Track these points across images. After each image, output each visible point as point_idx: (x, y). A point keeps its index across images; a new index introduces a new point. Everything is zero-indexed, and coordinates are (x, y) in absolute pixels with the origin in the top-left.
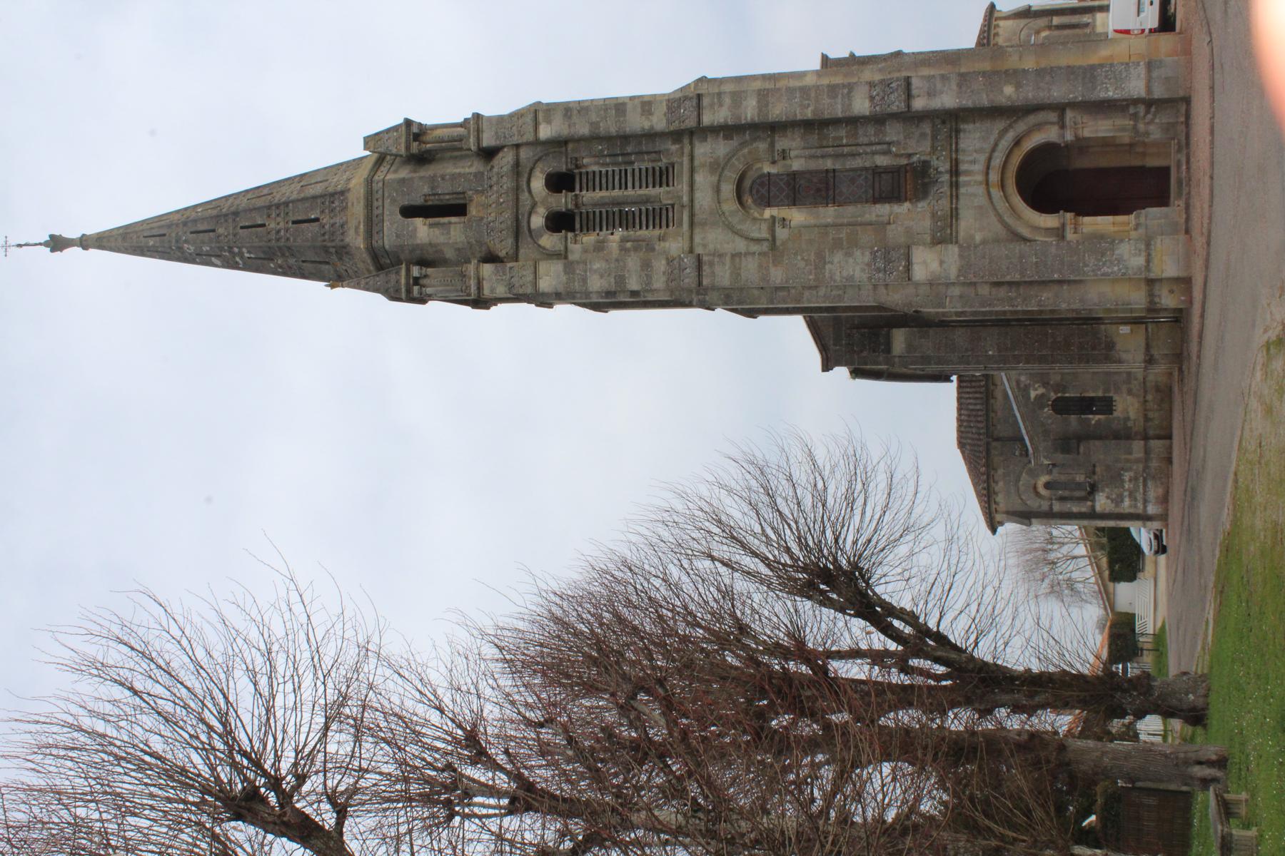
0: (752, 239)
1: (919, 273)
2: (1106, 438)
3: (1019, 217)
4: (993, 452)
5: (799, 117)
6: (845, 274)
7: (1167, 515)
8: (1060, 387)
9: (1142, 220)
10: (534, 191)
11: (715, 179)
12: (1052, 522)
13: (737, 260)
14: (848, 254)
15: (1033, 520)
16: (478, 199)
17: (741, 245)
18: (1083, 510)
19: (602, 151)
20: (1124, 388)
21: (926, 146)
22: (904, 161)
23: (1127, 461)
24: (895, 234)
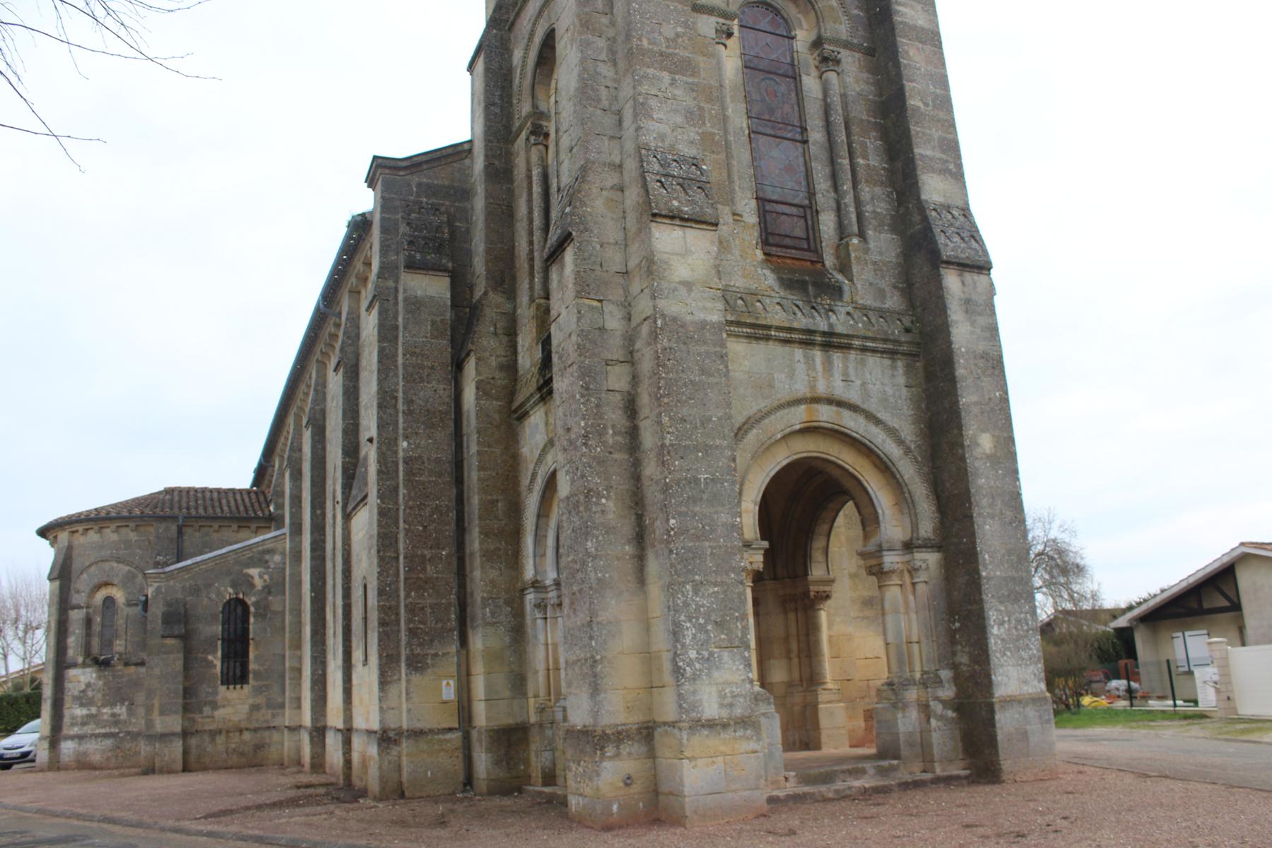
1: (666, 238)
2: (187, 677)
4: (162, 527)
5: (908, 86)
6: (653, 103)
7: (59, 769)
12: (54, 610)
15: (57, 583)
18: (71, 652)
20: (261, 700)
21: (867, 299)
22: (829, 260)
23: (149, 710)
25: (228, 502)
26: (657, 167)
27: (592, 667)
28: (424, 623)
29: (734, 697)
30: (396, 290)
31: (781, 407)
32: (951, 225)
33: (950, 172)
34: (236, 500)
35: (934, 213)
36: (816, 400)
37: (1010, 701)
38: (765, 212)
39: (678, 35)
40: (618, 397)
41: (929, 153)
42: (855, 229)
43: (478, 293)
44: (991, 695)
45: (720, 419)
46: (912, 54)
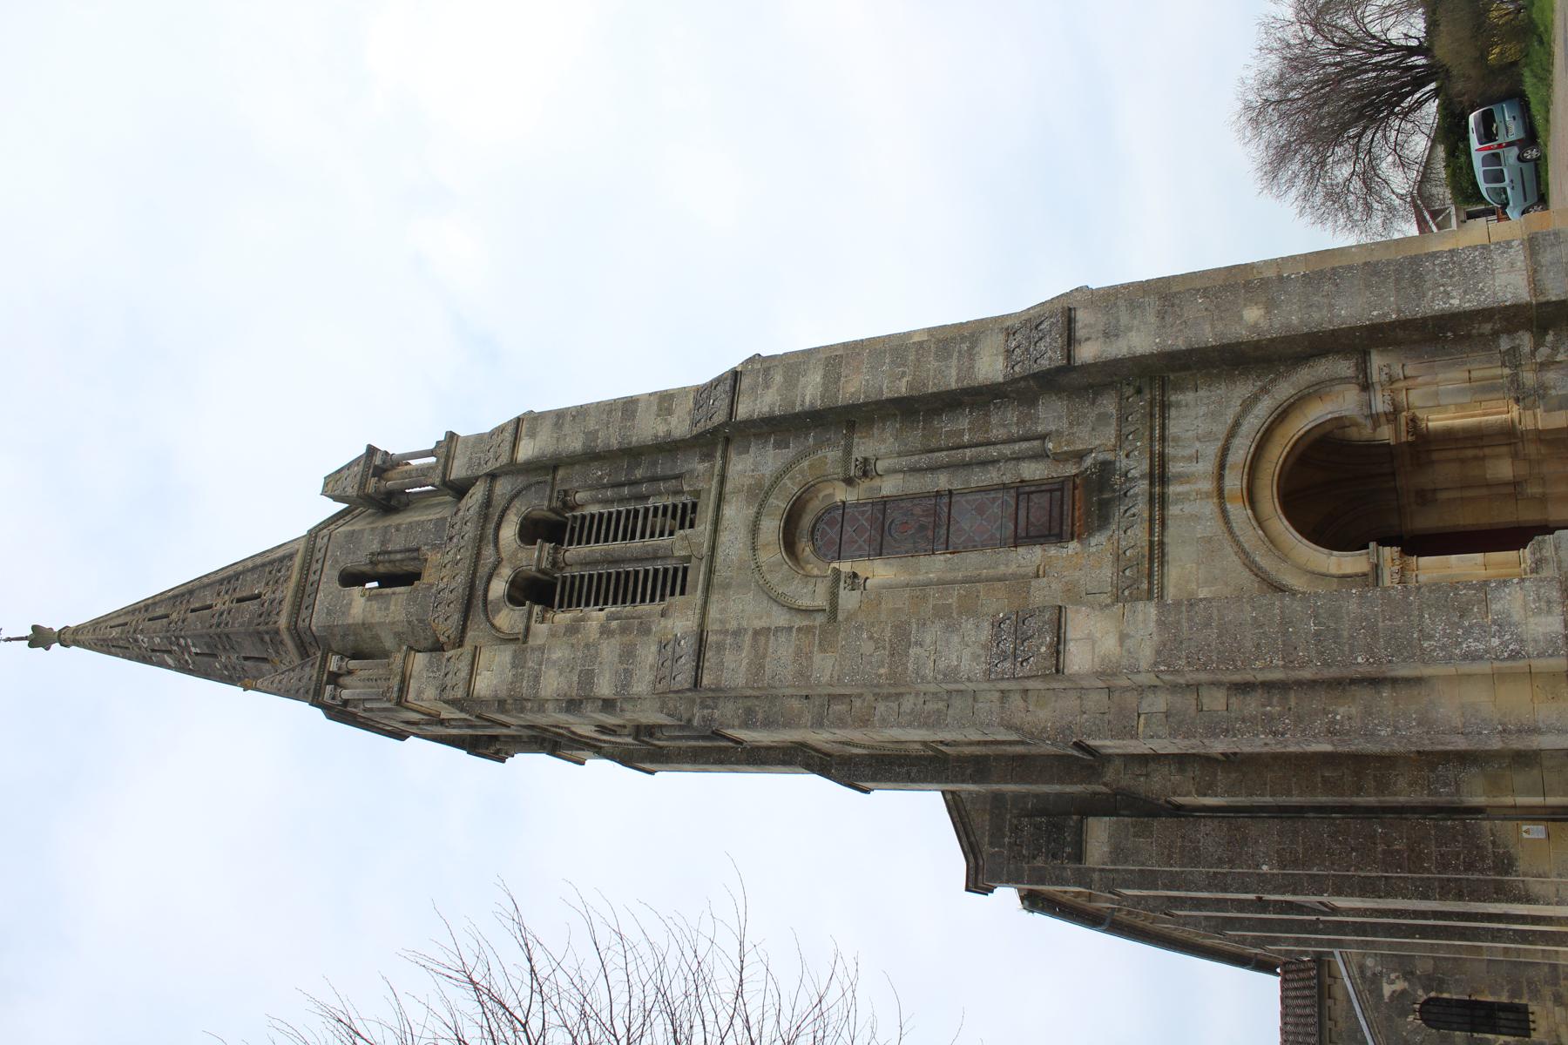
0: (799, 610)
1: (1078, 659)
3: (1284, 557)
5: (886, 395)
6: (942, 665)
8: (1430, 981)
9: (1548, 552)
10: (502, 542)
11: (752, 511)
13: (762, 639)
14: (951, 628)
16: (434, 558)
17: (780, 618)
19: (601, 478)
20: (1547, 991)
21: (1109, 434)
22: (1071, 469)
24: (1043, 594)
25: (1298, 1006)
26: (1007, 665)
27: (1510, 733)
28: (1458, 854)
29: (1539, 599)
30: (1102, 870)
31: (1230, 531)
32: (1027, 350)
33: (971, 349)
34: (1297, 997)
35: (1017, 369)
36: (1220, 493)
37: (1535, 284)
38: (1027, 536)
39: (871, 638)
40: (1233, 700)
41: (954, 372)
42: (1036, 443)
43: (1104, 789)
44: (1528, 306)
45: (1254, 608)
46: (855, 387)
